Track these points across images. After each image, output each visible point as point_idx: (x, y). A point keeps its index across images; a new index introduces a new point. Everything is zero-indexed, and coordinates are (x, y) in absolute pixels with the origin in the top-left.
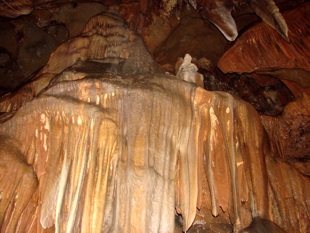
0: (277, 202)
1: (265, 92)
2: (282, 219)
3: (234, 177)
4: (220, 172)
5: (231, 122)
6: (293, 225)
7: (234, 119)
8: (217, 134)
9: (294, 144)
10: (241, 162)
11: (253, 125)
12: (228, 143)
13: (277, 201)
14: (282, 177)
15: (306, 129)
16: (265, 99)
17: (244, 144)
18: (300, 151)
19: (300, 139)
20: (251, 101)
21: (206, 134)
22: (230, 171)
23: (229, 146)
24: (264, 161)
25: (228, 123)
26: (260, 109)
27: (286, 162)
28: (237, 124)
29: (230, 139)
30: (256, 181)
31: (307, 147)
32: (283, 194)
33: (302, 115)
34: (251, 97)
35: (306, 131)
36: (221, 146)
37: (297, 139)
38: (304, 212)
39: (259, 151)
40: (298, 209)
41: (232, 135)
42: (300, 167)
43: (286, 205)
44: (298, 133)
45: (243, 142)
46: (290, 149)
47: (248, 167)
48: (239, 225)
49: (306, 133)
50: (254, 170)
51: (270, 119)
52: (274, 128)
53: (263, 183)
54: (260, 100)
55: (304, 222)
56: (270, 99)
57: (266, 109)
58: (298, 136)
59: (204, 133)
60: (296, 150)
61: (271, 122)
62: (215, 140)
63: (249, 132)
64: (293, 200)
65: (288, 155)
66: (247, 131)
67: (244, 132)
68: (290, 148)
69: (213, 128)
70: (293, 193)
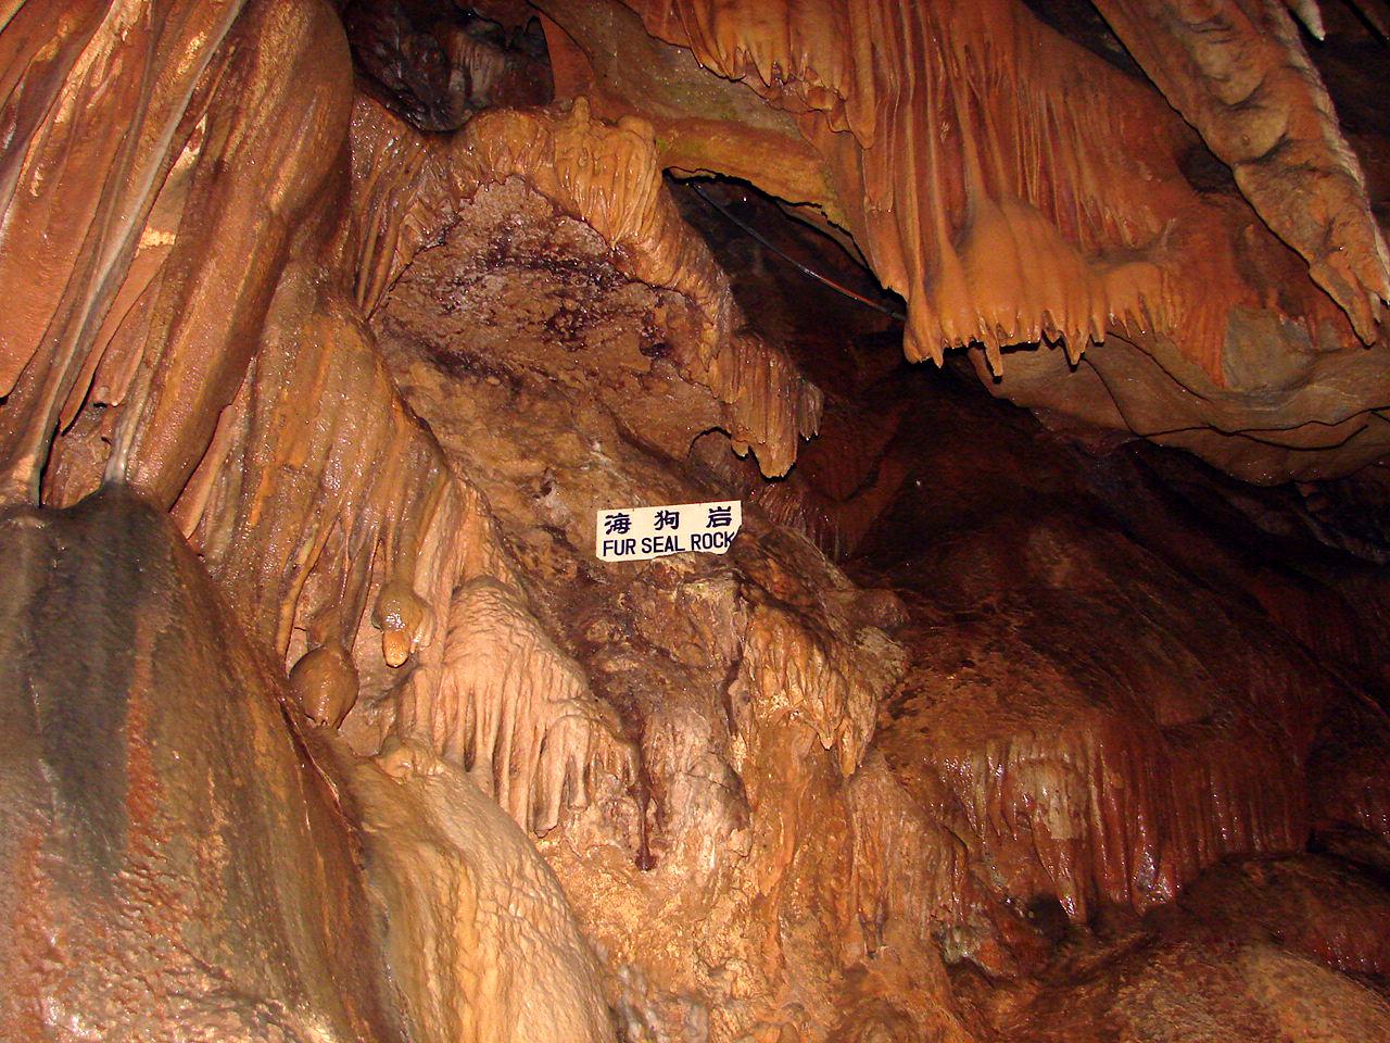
0: (245, 467)
1: (460, 38)
2: (234, 542)
3: (101, 278)
4: (50, 228)
5: (208, 43)
6: (267, 582)
7: (227, 41)
8: (119, 62)
9: (448, 284)
10: (171, 233)
11: (304, 111)
12: (148, 122)
13: (248, 461)
14: (315, 376)
15: (518, 248)
16: (447, 66)
17: (219, 164)
18: (460, 326)
19: (478, 279)
20: (381, 37)
21: (63, 35)
22: (96, 246)
23: (147, 138)
24: (272, 280)
25: (196, 42)
26: (398, 87)
27: (365, 328)
28: (234, 66)
29: (165, 112)
30: (191, 336)
31: (491, 323)
32: (287, 445)
33: (529, 183)
34: (388, 20)
35: (516, 257)
36: (111, 125)
37: (466, 272)
38: (336, 550)
39: (270, 228)
40: (316, 526)
41: (185, 103)
42: (422, 387)
43: (276, 494)
44: (482, 249)
45: (218, 154)
46: (420, 298)
47: (184, 265)
48: (21, 482)
49: (511, 263)
50: (202, 291)
51: (395, 131)
52: (392, 174)
53: (215, 360)
54: (424, 58)
55: (320, 586)
56: (468, 78)
57: (423, 104)
58: (477, 261)
59: (56, 23)
60: (444, 314)
61: (393, 147)
62: (94, 85)
63: (267, 130)
64: (315, 485)
65: (403, 319)
66: (261, 120)
67: (248, 116)
68: (425, 295)
69: (117, 26)
70: (328, 458)
